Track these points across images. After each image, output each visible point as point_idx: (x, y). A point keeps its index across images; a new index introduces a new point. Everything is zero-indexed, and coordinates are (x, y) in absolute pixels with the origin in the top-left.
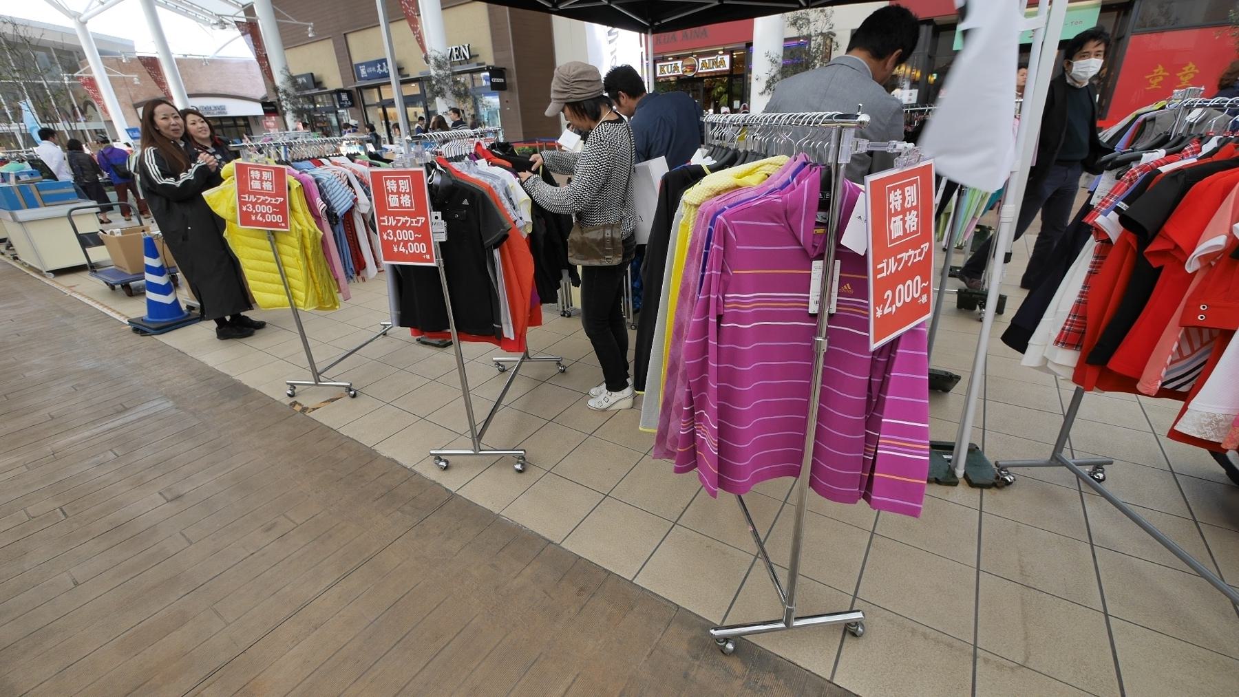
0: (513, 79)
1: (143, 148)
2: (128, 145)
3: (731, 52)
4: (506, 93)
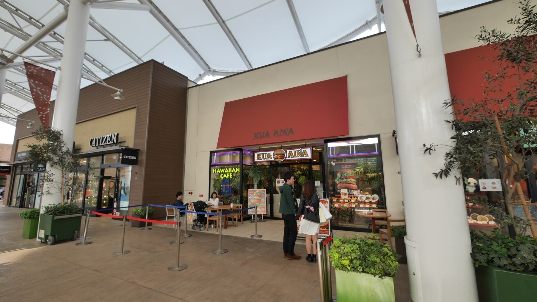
0: (143, 158)
1: (375, 203)
2: (490, 208)
3: (312, 146)
4: (136, 167)
